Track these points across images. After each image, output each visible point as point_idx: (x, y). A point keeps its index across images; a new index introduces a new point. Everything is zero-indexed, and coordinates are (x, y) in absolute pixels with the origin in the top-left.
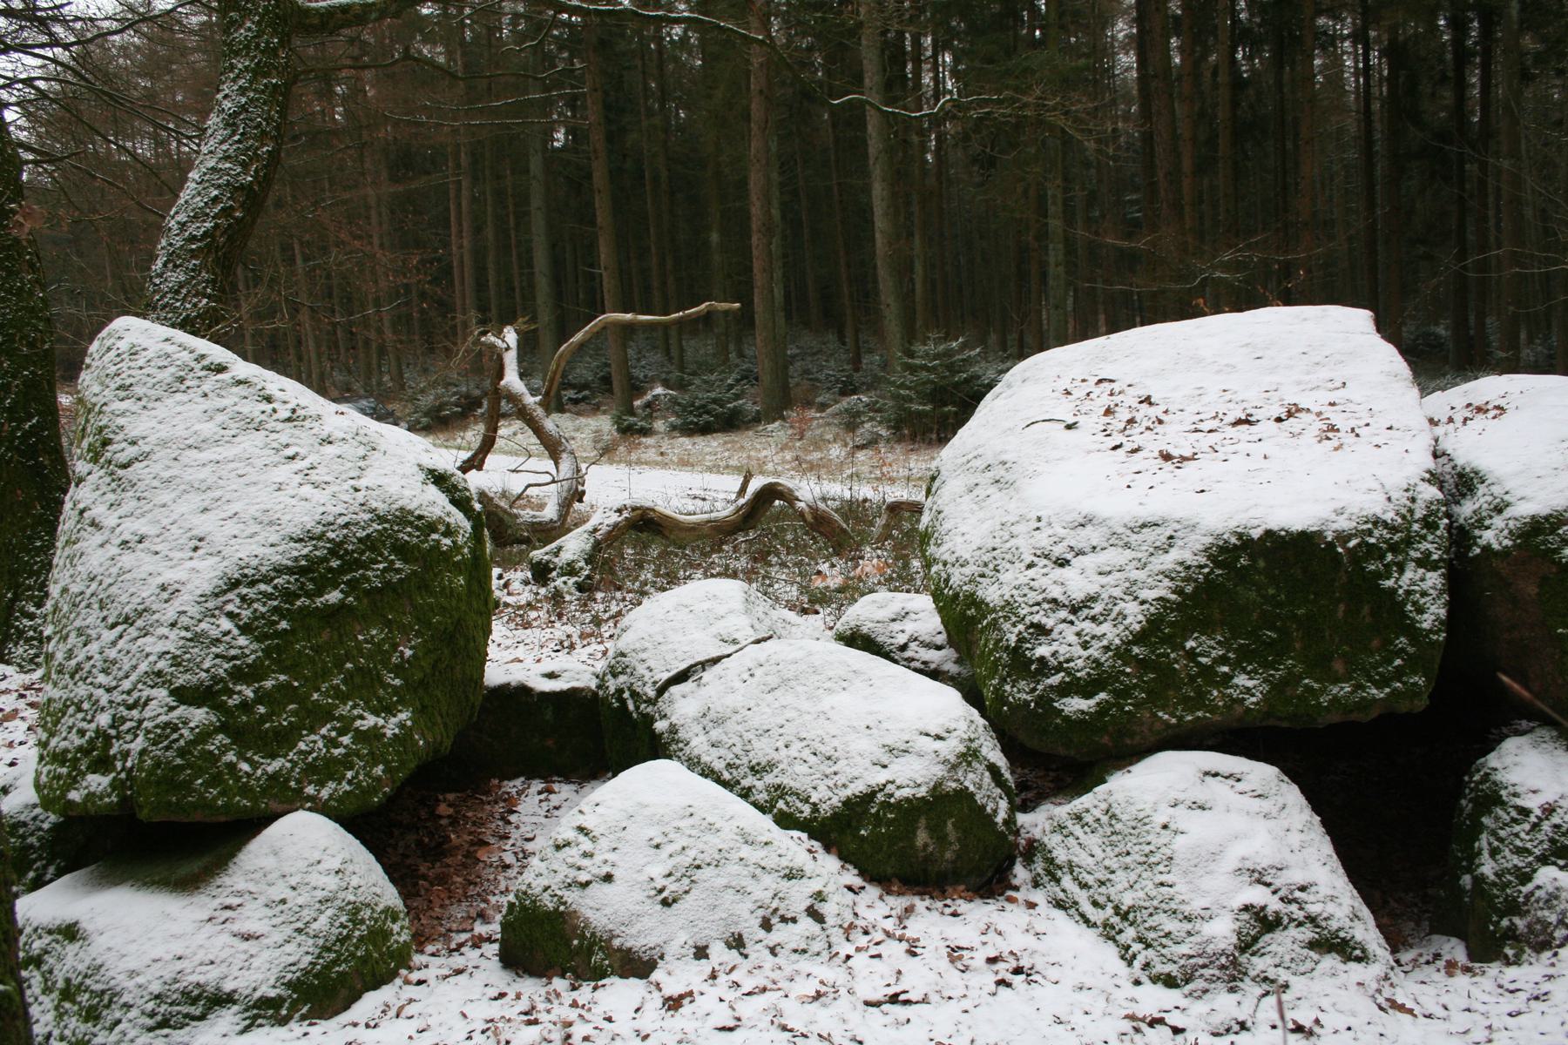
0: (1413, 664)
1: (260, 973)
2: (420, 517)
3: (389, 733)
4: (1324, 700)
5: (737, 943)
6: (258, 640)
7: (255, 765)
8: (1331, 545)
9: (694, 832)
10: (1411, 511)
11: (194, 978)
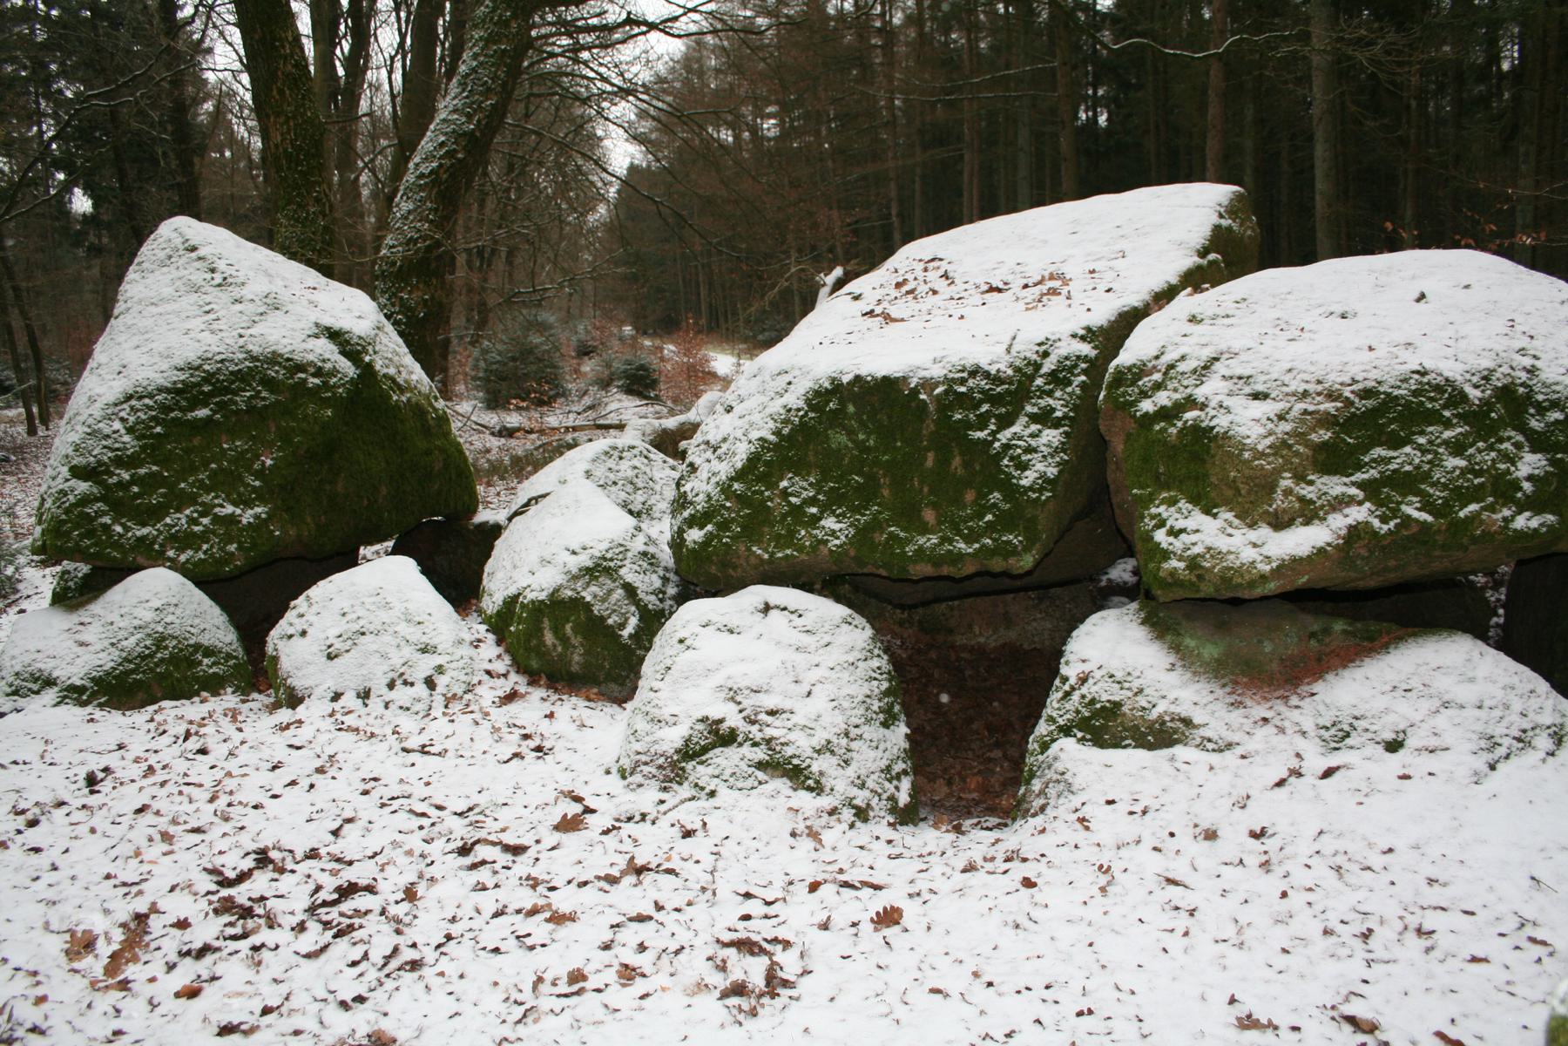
0: (1007, 521)
1: (75, 668)
2: (289, 360)
3: (245, 521)
4: (910, 550)
5: (365, 695)
6: (138, 438)
10: (1037, 367)
11: (39, 665)
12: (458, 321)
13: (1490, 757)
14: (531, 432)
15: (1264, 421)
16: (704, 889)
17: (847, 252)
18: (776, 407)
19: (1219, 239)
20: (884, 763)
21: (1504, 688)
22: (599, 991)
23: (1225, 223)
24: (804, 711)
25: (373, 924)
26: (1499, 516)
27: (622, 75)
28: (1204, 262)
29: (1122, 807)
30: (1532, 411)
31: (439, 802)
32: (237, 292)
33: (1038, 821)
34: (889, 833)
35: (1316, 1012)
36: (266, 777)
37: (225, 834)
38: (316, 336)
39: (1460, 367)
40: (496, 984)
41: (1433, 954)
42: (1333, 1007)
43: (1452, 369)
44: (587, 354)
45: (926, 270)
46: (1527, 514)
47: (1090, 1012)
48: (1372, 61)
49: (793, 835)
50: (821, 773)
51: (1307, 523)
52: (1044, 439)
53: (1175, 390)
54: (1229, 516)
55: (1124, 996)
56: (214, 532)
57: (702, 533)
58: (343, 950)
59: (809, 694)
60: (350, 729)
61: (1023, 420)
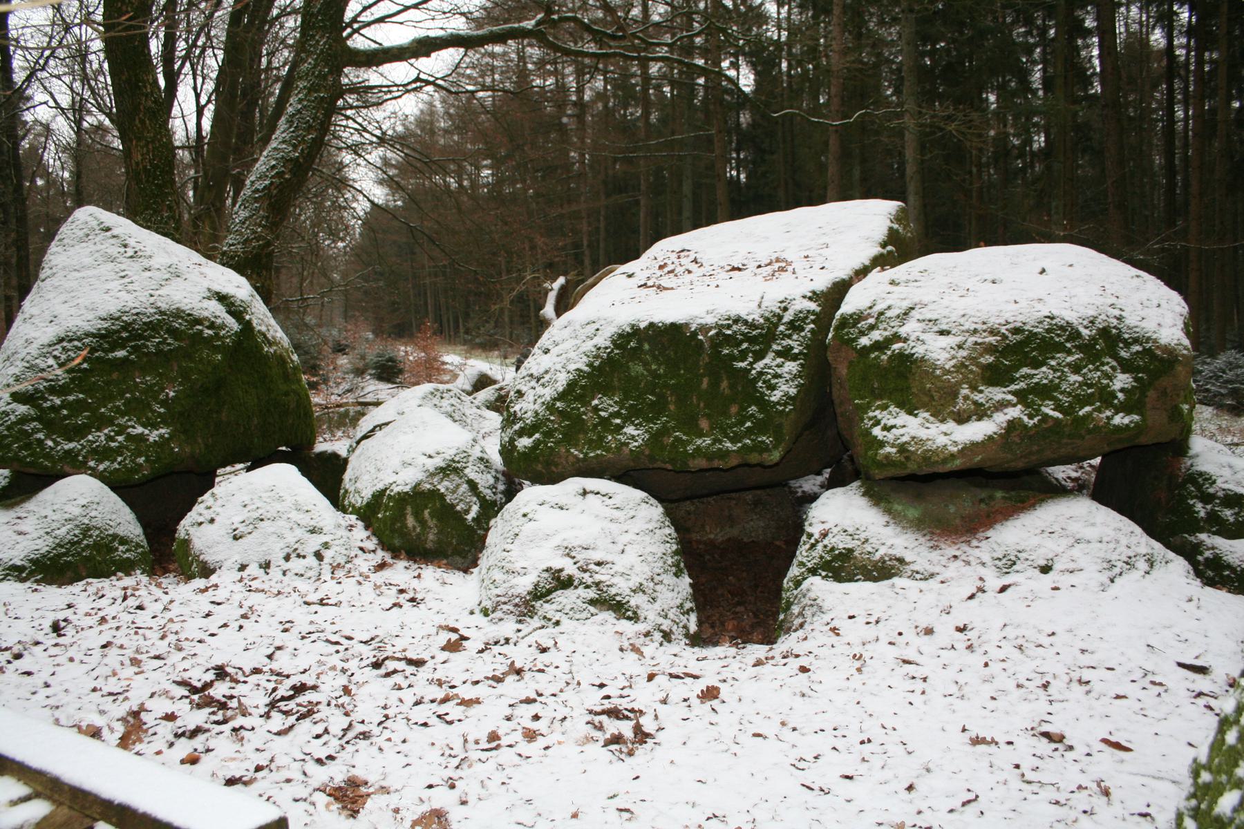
0: (760, 427)
2: (189, 315)
3: (151, 439)
4: (690, 448)
5: (266, 566)
7: (57, 443)
8: (695, 334)
10: (780, 318)
18: (589, 346)
19: (892, 237)
20: (679, 602)
22: (510, 746)
23: (896, 226)
24: (622, 563)
25: (324, 711)
26: (1103, 416)
28: (885, 251)
29: (861, 620)
31: (348, 634)
33: (800, 633)
35: (1021, 733)
38: (209, 298)
43: (1069, 315)
44: (339, 351)
47: (869, 741)
49: (621, 650)
50: (638, 607)
51: (979, 419)
53: (885, 329)
54: (927, 415)
56: (127, 448)
57: (531, 440)
60: (257, 590)
61: (771, 355)
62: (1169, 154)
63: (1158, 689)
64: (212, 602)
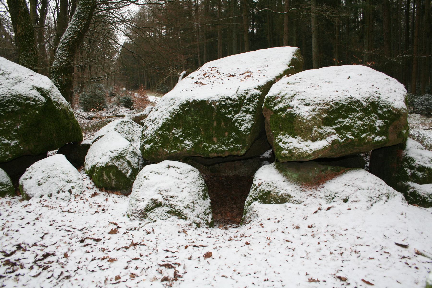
0: (237, 141)
2: (24, 96)
3: (12, 145)
4: (210, 149)
5: (50, 196)
8: (210, 104)
9: (52, 170)
12: (75, 86)
13: (371, 203)
14: (97, 118)
15: (309, 111)
16: (154, 249)
17: (186, 67)
18: (171, 109)
19: (293, 62)
20: (204, 210)
21: (374, 184)
22: (124, 282)
23: (295, 57)
24: (181, 196)
26: (371, 137)
27: (122, 16)
28: (289, 68)
29: (272, 220)
30: (379, 108)
31: (74, 227)
32: (8, 76)
33: (249, 225)
34: (206, 230)
35: (330, 276)
36: (20, 222)
37: (7, 240)
38: (33, 90)
39: (360, 97)
40: (93, 281)
41: (360, 258)
42: (334, 274)
43: (358, 97)
44: (113, 96)
45: (212, 70)
46: (378, 136)
47: (268, 280)
48: (328, 16)
49: (179, 232)
50: (186, 214)
51: (321, 140)
52: (247, 117)
53: (284, 103)
54: (300, 138)
55: (277, 275)
57: (150, 146)
58: (45, 274)
59: (182, 191)
60: (46, 206)
61: (241, 112)
62: (407, 22)
63: (387, 255)
64: (27, 212)
